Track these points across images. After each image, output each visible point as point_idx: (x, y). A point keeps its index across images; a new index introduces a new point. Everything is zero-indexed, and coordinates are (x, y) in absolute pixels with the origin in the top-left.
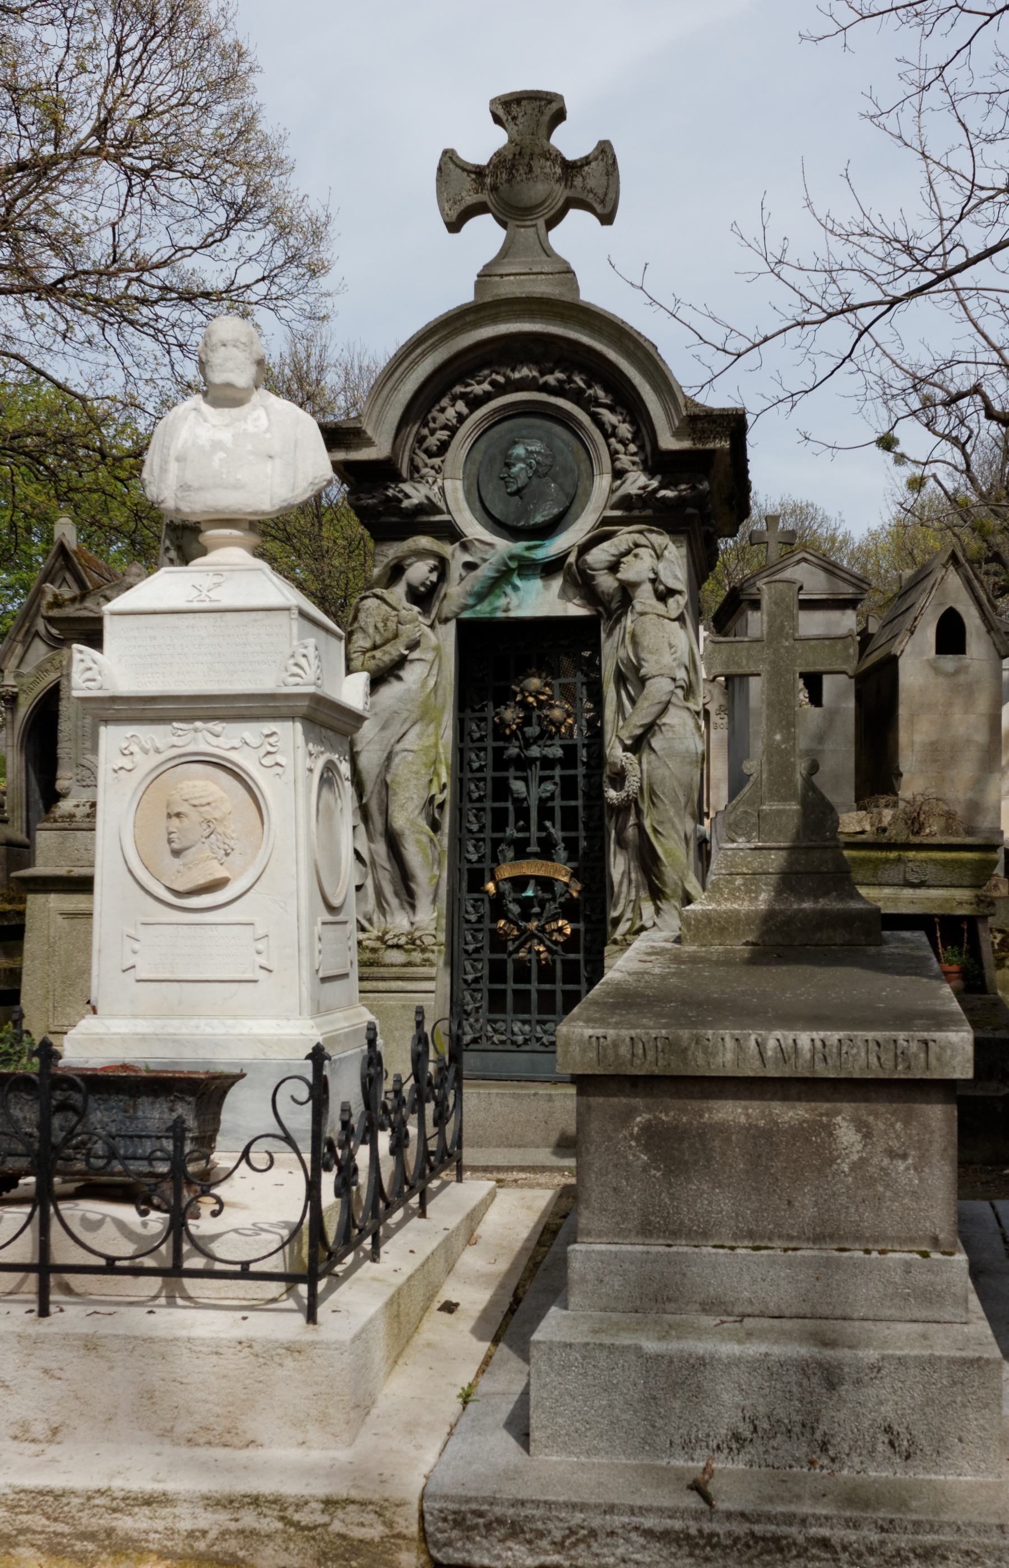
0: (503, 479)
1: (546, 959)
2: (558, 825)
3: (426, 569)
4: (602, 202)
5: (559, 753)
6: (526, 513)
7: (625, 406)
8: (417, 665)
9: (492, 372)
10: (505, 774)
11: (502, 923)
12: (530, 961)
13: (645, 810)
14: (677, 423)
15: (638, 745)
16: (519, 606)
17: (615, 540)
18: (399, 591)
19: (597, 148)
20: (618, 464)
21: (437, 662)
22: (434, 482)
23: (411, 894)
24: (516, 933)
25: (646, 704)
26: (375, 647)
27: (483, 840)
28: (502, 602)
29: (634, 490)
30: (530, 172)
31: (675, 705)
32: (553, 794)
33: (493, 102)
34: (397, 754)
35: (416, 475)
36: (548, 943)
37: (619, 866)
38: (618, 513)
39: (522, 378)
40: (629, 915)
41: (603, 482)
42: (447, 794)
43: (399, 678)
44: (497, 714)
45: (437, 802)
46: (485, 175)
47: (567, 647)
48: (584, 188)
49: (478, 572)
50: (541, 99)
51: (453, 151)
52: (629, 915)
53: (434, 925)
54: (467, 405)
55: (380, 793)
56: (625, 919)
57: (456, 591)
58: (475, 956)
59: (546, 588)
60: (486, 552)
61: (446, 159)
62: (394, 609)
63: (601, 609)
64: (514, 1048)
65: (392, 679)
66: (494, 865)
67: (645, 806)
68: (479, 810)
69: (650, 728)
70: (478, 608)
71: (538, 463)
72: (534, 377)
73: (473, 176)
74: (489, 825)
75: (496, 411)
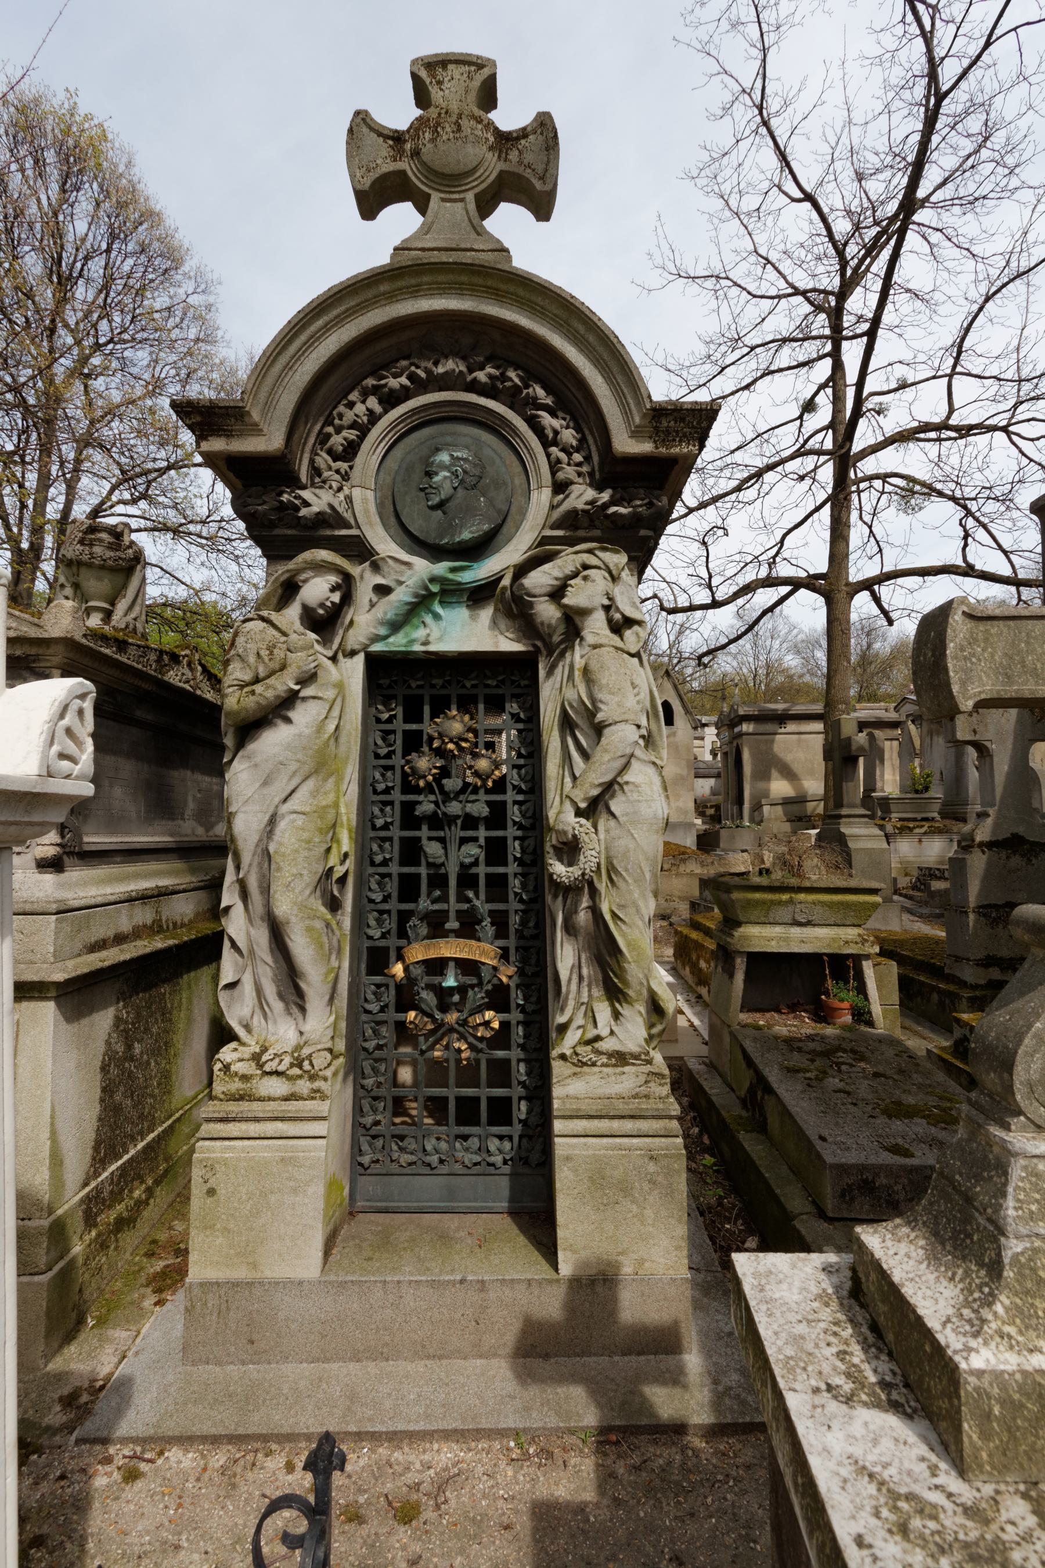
0: (422, 490)
1: (467, 1059)
2: (482, 896)
3: (326, 587)
4: (542, 178)
5: (485, 811)
6: (450, 527)
7: (567, 411)
8: (312, 705)
9: (412, 364)
10: (417, 833)
11: (412, 1015)
12: (447, 1060)
13: (603, 891)
14: (637, 420)
15: (594, 808)
16: (440, 639)
17: (558, 562)
18: (293, 613)
19: (535, 119)
20: (561, 475)
21: (339, 702)
22: (340, 489)
23: (300, 994)
24: (430, 1026)
25: (606, 757)
26: (257, 680)
27: (388, 912)
28: (420, 633)
29: (580, 505)
30: (457, 149)
31: (639, 759)
32: (477, 859)
33: (414, 62)
34: (283, 816)
35: (317, 480)
36: (471, 1039)
37: (567, 957)
38: (560, 533)
39: (446, 373)
40: (579, 1020)
41: (542, 498)
42: (349, 864)
43: (288, 720)
44: (408, 762)
45: (336, 875)
46: (405, 141)
47: (500, 683)
48: (520, 163)
49: (392, 597)
50: (470, 63)
51: (366, 112)
52: (579, 1020)
53: (330, 1033)
54: (380, 402)
55: (260, 865)
56: (574, 1025)
57: (364, 622)
58: (378, 1054)
59: (473, 618)
60: (402, 573)
61: (358, 120)
62: (285, 634)
63: (539, 643)
64: (427, 1170)
65: (279, 722)
66: (403, 942)
67: (602, 885)
68: (383, 876)
69: (609, 788)
70: (391, 640)
71: (465, 472)
72: (461, 372)
73: (391, 142)
74: (395, 895)
75: (414, 411)
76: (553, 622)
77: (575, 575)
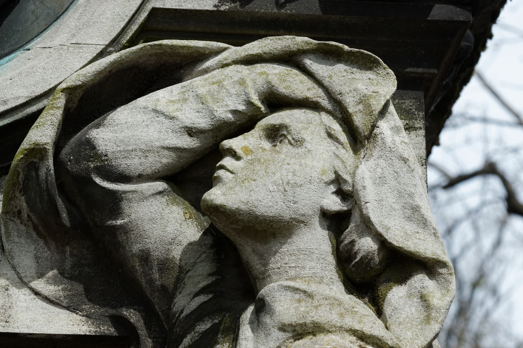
17: (197, 84)
63: (132, 316)
76: (177, 253)
77: (244, 124)
